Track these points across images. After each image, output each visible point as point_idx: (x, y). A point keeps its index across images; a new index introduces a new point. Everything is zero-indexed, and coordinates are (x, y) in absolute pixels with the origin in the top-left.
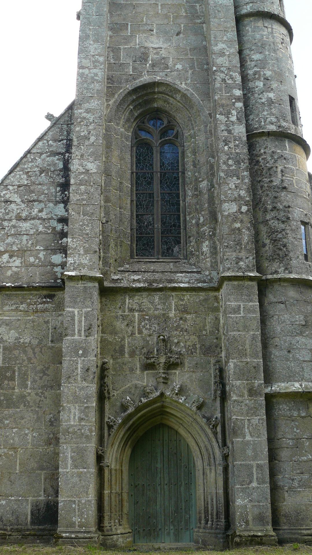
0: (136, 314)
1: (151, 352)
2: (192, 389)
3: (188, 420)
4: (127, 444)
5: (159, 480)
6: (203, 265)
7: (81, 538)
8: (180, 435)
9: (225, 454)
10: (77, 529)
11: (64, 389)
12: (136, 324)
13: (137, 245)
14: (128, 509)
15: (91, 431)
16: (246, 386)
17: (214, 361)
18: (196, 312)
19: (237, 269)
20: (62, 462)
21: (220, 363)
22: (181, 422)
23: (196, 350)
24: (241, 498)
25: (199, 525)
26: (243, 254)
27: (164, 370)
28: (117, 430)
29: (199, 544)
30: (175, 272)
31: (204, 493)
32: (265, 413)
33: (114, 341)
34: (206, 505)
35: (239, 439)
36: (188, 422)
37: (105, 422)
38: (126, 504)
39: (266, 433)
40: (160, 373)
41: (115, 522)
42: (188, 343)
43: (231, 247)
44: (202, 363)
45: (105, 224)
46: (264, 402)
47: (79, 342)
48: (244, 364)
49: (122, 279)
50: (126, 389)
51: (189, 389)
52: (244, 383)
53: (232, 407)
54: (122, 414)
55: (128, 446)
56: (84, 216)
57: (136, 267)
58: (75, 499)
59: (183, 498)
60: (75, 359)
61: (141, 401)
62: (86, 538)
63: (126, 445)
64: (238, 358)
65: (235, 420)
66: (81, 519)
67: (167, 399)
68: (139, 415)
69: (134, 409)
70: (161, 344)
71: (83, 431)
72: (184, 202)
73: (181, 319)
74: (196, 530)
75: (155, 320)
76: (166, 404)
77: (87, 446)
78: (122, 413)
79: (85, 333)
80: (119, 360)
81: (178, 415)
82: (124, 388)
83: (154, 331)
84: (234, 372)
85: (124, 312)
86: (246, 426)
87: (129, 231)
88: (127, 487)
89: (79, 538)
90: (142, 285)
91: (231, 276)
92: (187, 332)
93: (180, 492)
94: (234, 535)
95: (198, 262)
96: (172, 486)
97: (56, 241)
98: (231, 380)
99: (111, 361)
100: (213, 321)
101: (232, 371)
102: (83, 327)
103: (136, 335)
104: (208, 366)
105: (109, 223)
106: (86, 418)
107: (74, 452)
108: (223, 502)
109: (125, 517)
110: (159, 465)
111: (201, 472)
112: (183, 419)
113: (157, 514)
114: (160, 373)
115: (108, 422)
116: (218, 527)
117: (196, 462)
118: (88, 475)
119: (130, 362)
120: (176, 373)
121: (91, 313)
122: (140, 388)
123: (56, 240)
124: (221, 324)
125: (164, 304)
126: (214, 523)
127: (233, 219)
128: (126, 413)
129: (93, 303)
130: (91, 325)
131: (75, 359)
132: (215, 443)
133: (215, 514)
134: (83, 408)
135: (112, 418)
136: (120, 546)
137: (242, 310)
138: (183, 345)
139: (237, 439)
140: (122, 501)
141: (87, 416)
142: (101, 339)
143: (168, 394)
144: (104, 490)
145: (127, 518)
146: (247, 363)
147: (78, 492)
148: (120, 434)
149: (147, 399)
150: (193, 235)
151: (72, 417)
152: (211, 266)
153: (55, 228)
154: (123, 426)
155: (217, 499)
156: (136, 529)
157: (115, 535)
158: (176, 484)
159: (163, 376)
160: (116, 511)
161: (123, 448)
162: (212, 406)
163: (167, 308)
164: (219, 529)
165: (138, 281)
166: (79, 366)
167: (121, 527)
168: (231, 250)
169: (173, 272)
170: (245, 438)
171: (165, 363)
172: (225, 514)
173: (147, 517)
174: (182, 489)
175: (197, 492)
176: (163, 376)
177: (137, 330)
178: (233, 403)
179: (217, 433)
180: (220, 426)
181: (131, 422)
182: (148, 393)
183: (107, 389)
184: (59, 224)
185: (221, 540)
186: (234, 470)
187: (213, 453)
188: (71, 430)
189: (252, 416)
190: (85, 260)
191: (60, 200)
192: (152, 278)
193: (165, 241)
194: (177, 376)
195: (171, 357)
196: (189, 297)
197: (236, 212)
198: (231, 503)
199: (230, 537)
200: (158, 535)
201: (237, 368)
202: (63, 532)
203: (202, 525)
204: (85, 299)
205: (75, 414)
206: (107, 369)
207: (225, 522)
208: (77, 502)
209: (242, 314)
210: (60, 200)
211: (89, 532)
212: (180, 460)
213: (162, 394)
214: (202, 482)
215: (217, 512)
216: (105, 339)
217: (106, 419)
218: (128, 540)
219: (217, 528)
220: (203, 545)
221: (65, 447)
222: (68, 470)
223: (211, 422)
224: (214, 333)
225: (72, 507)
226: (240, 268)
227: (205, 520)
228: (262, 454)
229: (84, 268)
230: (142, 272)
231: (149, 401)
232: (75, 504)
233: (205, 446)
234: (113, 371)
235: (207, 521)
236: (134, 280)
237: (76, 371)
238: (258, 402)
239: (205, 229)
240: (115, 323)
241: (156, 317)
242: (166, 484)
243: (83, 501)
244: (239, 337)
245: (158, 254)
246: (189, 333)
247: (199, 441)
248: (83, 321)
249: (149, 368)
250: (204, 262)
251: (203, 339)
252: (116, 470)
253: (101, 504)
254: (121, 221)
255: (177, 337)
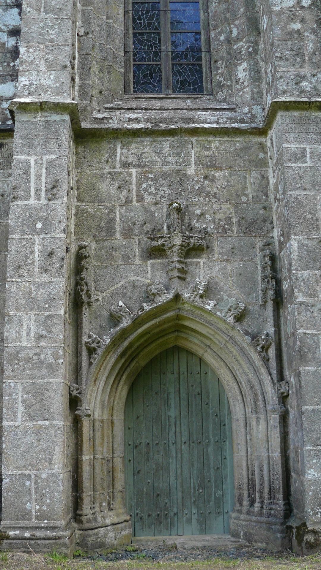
0: (134, 171)
2: (226, 288)
3: (221, 339)
4: (121, 379)
5: (174, 436)
6: (238, 98)
7: (40, 539)
8: (207, 364)
9: (283, 393)
10: (34, 522)
11: (10, 287)
12: (134, 187)
13: (134, 76)
14: (123, 484)
15: (56, 356)
17: (261, 244)
18: (230, 167)
19: (297, 93)
20: (8, 410)
21: (270, 247)
22: (209, 343)
23: (232, 226)
24: (316, 468)
25: (239, 508)
26: (306, 70)
27: (180, 257)
28: (102, 357)
29: (240, 538)
30: (195, 109)
31: (247, 456)
33: (98, 213)
34: (250, 477)
35: (310, 368)
36: (219, 342)
37: (83, 343)
38: (120, 476)
40: (172, 262)
41: (101, 506)
42: (219, 216)
43: (287, 60)
44: (241, 246)
45: (84, 37)
47: (36, 209)
48: (314, 243)
49: (111, 118)
50: (117, 289)
51: (222, 289)
52: (316, 274)
53: (296, 313)
54: (112, 330)
56: (47, 13)
57: (133, 105)
58: (30, 473)
59: (212, 464)
60: (30, 236)
61: (142, 308)
62: (49, 539)
63: (120, 381)
64: (304, 233)
65: (302, 335)
66: (41, 506)
67: (186, 305)
68: (140, 331)
69: (130, 321)
70: (175, 216)
71: (42, 357)
72: (206, 14)
73: (206, 177)
74: (234, 515)
75: (163, 180)
76: (184, 314)
77: (50, 383)
78: (111, 328)
79: (46, 194)
80: (106, 244)
82: (114, 288)
83: (163, 197)
84: (298, 256)
85: (114, 168)
87: (122, 53)
88: (122, 447)
89: (38, 539)
90: (142, 126)
91: (290, 102)
92: (215, 198)
93: (207, 454)
94: (302, 529)
95: (231, 96)
96: (195, 445)
97: (6, 64)
99: (93, 245)
100: (257, 182)
101: (296, 254)
102: (44, 185)
104: (251, 251)
105: (90, 36)
106: (48, 335)
107: (28, 393)
108: (280, 472)
109: (118, 496)
110: (172, 413)
111: (242, 423)
112: (212, 338)
113: (170, 489)
114: (172, 262)
115: (88, 342)
116: (273, 512)
117: (232, 407)
118: (52, 432)
119: (123, 246)
120: (199, 263)
121: (57, 162)
122: (141, 287)
123: (5, 62)
124: (271, 186)
125: (179, 155)
126: (264, 507)
127: (289, 16)
128: (118, 329)
129: (60, 146)
130: (57, 181)
131: (30, 236)
133: (266, 491)
134: (42, 318)
135: (95, 336)
136: (110, 544)
137: (308, 156)
138: (210, 219)
140: (113, 471)
141: (50, 332)
142: (77, 211)
143: (188, 295)
144: (82, 454)
145: (122, 498)
147: (34, 460)
148: (108, 363)
149: (151, 305)
150: (222, 58)
151: (25, 333)
152: (253, 98)
153: (4, 44)
154: (113, 350)
155: (269, 467)
156: (137, 514)
157: (102, 527)
158: (200, 443)
159: (179, 266)
160: (103, 488)
161: (115, 386)
162: (260, 315)
163: (184, 162)
164: (275, 516)
165: (137, 120)
166: (37, 248)
167: (111, 513)
168: (287, 63)
169: (191, 109)
171: (182, 246)
172: (284, 492)
173: (155, 495)
174: (211, 450)
175: (236, 454)
176: (179, 266)
177: (134, 196)
178: (298, 308)
179: (268, 360)
180: (274, 348)
181: (126, 344)
182: (154, 295)
183: (85, 288)
184: (10, 39)
185: (279, 535)
186: (302, 420)
187: (263, 392)
188: (22, 355)
190: (48, 80)
191: (12, 3)
192: (158, 117)
193: (178, 71)
194: (202, 267)
195: (192, 237)
196: (218, 145)
197: (293, 7)
198: (293, 474)
199: (294, 531)
200: (172, 524)
201: (303, 250)
202: (10, 527)
203: (245, 509)
204: (47, 140)
205: (29, 329)
206: (86, 257)
207: (284, 505)
208: (33, 477)
209: (309, 163)
210: (12, 3)
211: (54, 528)
212: (207, 404)
213: (177, 297)
214: (243, 439)
215: (270, 489)
216: (83, 210)
217: (85, 339)
218: (123, 533)
219: (270, 515)
220: (246, 540)
221: (12, 385)
222: (17, 424)
223: (258, 341)
224: (260, 200)
225: (25, 485)
226: (303, 91)
227: (249, 500)
229: (45, 92)
230: (142, 109)
232: (30, 480)
233: (249, 381)
234: (96, 261)
235: (252, 503)
236: (130, 120)
237: (31, 257)
239: (242, 45)
240: (99, 185)
241: (166, 175)
242: (185, 443)
243: (44, 476)
244: (306, 198)
245: (167, 88)
246: (219, 200)
248: (44, 175)
250: (240, 94)
251: (243, 209)
252: (102, 421)
253: (77, 477)
254: (108, 36)
255: (201, 205)
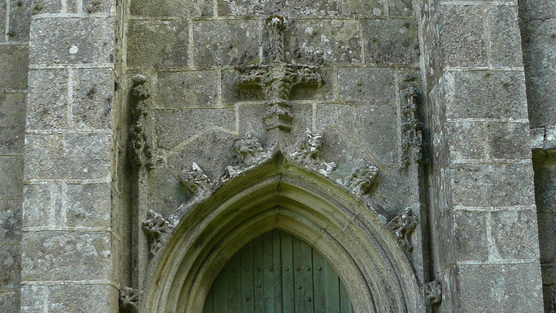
1: (251, 57)
2: (349, 144)
3: (342, 219)
4: (195, 278)
8: (322, 257)
9: (432, 299)
11: (31, 142)
15: (99, 245)
16: (486, 130)
22: (324, 225)
23: (359, 52)
27: (283, 97)
28: (168, 246)
32: (533, 198)
33: (162, 32)
35: (472, 262)
36: (340, 223)
37: (140, 225)
39: (536, 245)
40: (271, 105)
42: (339, 36)
44: (373, 81)
46: (530, 171)
47: (70, 26)
48: (479, 78)
51: (344, 146)
52: (481, 124)
53: (452, 181)
54: (181, 206)
55: (197, 284)
61: (226, 174)
63: (193, 282)
64: (464, 63)
65: (460, 213)
67: (291, 169)
68: (223, 207)
69: (209, 193)
70: (275, 36)
71: (79, 246)
76: (289, 182)
77: (91, 285)
78: (181, 202)
81: (317, 207)
82: (185, 143)
84: (456, 96)
86: (489, 229)
92: (335, 9)
98: (449, 117)
99: (155, 79)
101: (452, 93)
103: (214, 18)
104: (387, 89)
106: (87, 214)
107: (58, 301)
112: (329, 217)
114: (271, 105)
115: (147, 225)
119: (199, 81)
120: (311, 106)
128: (190, 204)
131: (61, 66)
132: (408, 273)
134: (79, 189)
135: (157, 215)
138: (327, 40)
139: (468, 262)
141: (91, 209)
142: (130, 28)
146: (488, 75)
148: (176, 255)
149: (240, 168)
151: (52, 211)
154: (184, 236)
161: (187, 289)
162: (399, 184)
166: (71, 84)
170: (487, 259)
171: (285, 81)
177: (216, 7)
178: (455, 173)
179: (411, 250)
181: (203, 226)
182: (244, 153)
183: (142, 143)
187: (403, 297)
188: (48, 244)
189: (502, 203)
195: (299, 68)
205: (59, 205)
206: (143, 97)
213: (278, 157)
216: (140, 26)
217: (142, 219)
221: (34, 288)
223: (396, 221)
228: (529, 297)
231: (246, 173)
233: (383, 281)
234: (159, 103)
237: (62, 97)
238: (515, 170)
246: (340, 13)
247: (367, 268)
249: (245, 94)
251: (375, 27)
255: (314, 21)
